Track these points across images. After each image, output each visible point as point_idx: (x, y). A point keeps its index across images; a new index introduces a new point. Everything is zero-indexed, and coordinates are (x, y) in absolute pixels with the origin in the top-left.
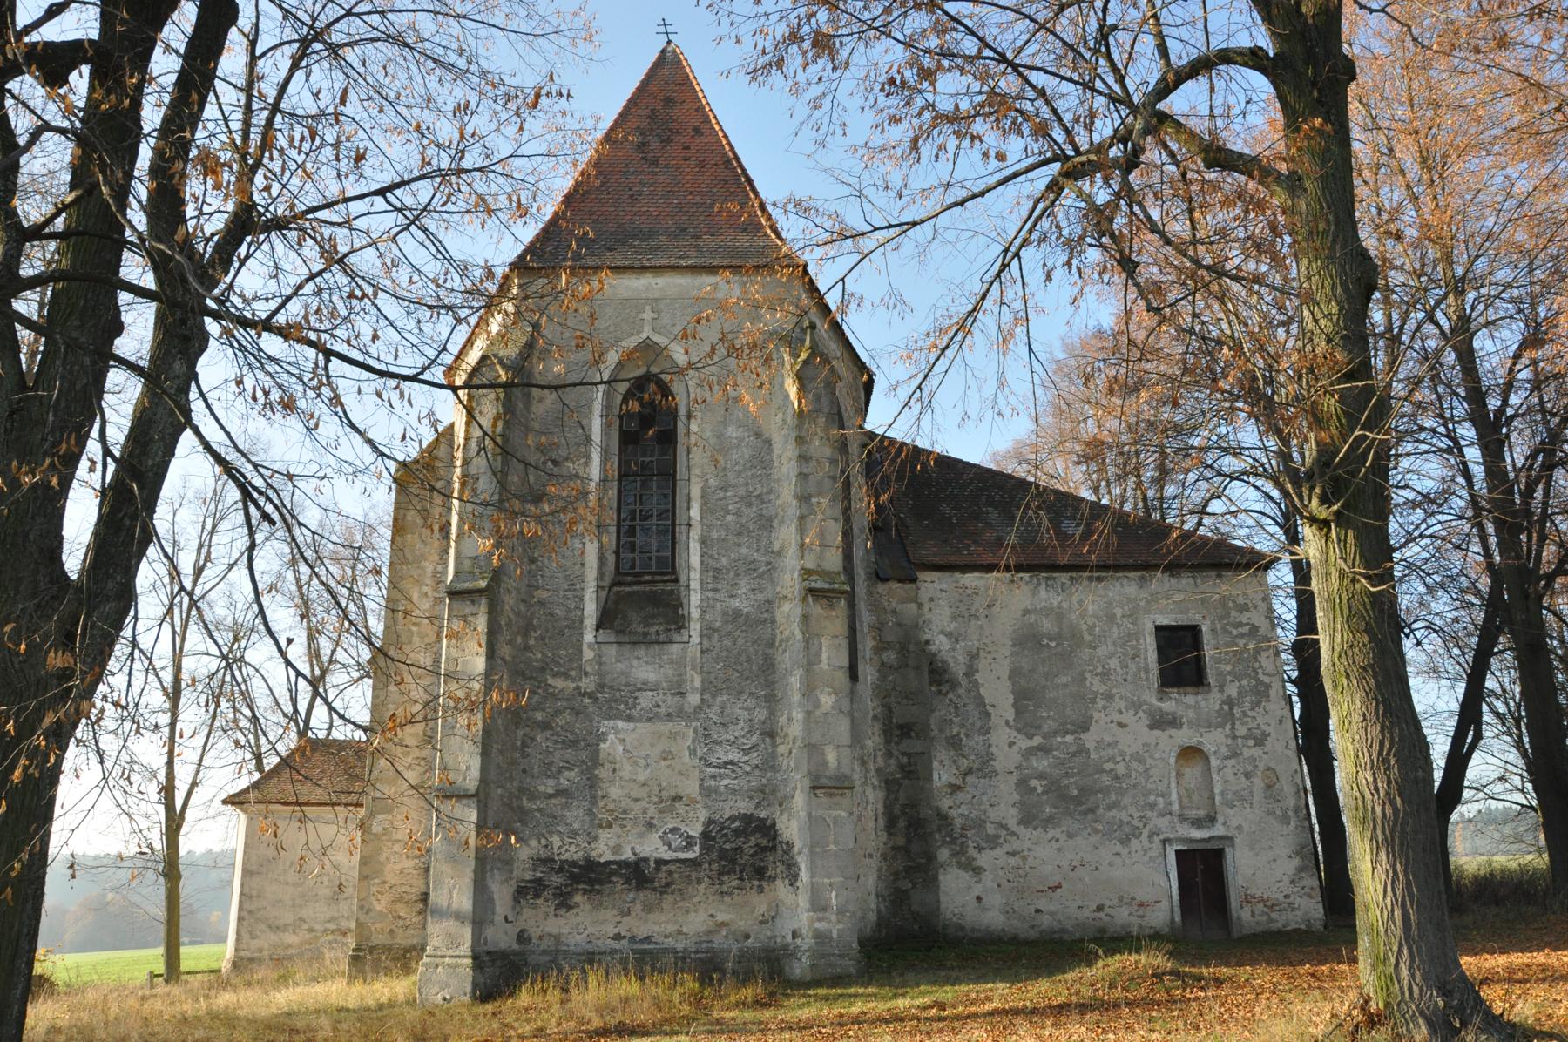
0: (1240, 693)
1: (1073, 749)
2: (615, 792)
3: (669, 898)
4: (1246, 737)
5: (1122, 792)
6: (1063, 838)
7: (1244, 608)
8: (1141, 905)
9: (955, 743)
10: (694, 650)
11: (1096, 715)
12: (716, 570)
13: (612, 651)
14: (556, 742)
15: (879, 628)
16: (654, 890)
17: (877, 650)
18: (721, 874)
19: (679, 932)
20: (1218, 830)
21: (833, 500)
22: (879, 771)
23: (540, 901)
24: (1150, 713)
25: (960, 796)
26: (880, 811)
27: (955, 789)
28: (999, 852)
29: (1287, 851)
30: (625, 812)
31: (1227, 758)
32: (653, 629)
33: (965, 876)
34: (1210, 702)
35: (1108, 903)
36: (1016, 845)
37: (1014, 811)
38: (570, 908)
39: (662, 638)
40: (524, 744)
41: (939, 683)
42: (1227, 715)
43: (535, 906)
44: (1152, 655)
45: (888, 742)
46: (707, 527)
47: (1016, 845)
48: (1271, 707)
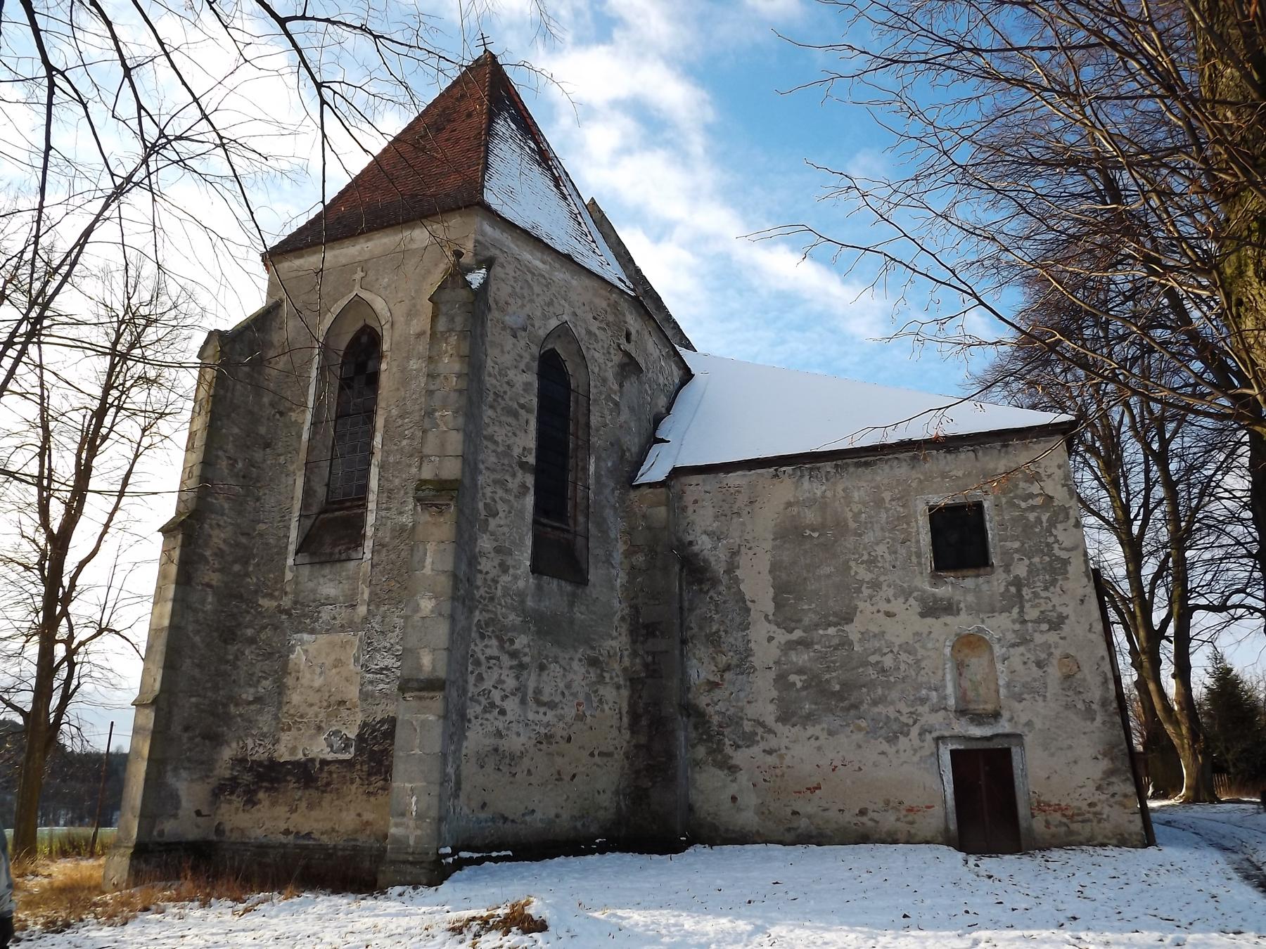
0: (1030, 572)
1: (836, 641)
2: (296, 698)
3: (328, 797)
4: (1038, 621)
5: (888, 686)
6: (823, 736)
7: (1036, 478)
8: (910, 810)
9: (714, 641)
10: (366, 566)
11: (861, 605)
12: (390, 491)
13: (306, 571)
14: (258, 655)
15: (630, 532)
16: (317, 789)
17: (628, 554)
18: (370, 774)
19: (333, 830)
20: (1004, 727)
21: (456, 412)
22: (625, 670)
23: (234, 797)
24: (922, 600)
25: (718, 694)
26: (625, 708)
27: (713, 686)
28: (756, 750)
29: (1091, 752)
30: (302, 717)
31: (1013, 645)
32: (337, 550)
33: (721, 774)
34: (995, 583)
35: (871, 807)
36: (773, 742)
37: (771, 708)
38: (255, 804)
39: (344, 556)
40: (236, 658)
41: (701, 582)
42: (1015, 596)
43: (230, 802)
44: (925, 538)
45: (634, 642)
46: (387, 453)
47: (773, 742)
48: (1068, 585)
